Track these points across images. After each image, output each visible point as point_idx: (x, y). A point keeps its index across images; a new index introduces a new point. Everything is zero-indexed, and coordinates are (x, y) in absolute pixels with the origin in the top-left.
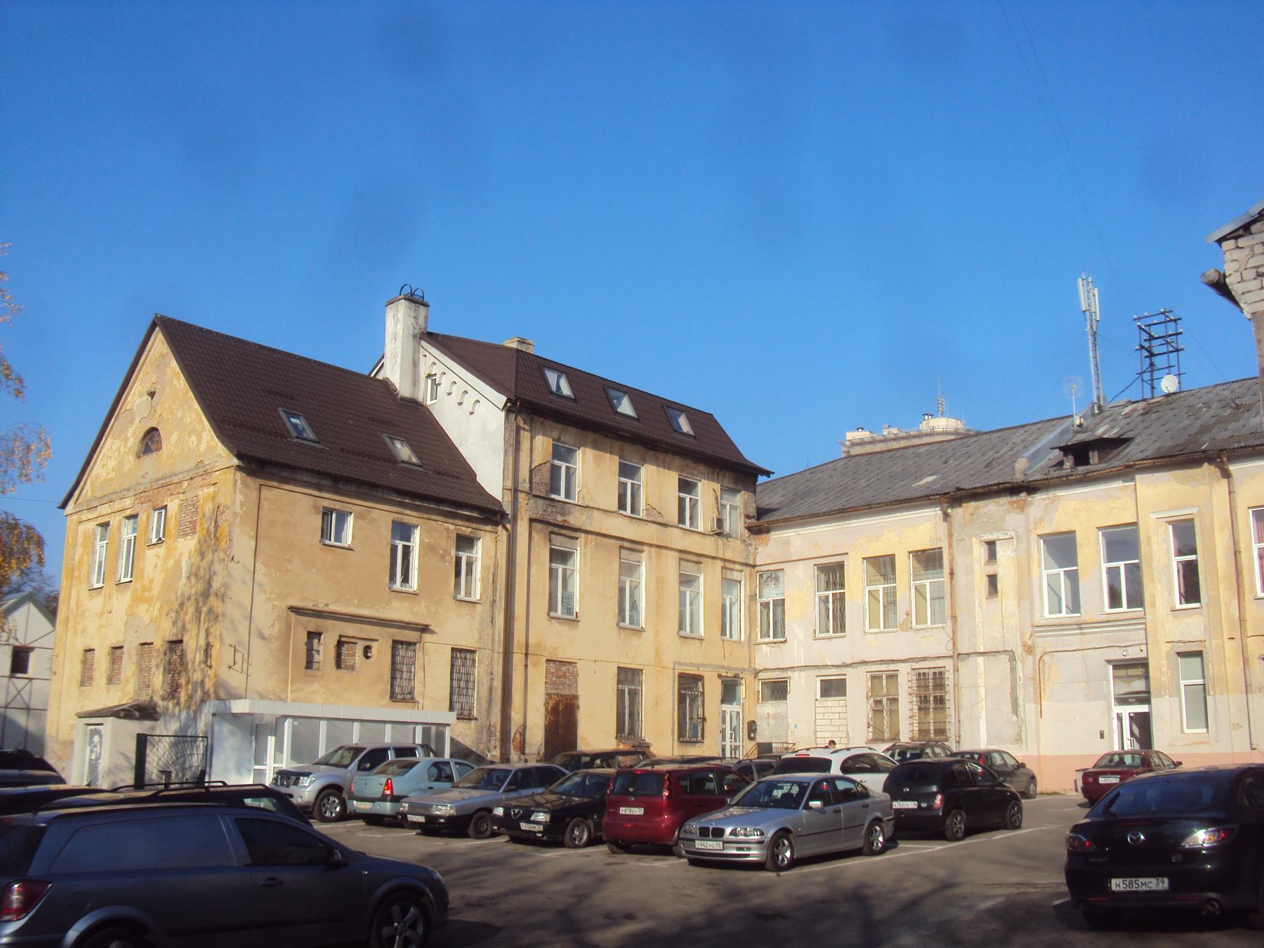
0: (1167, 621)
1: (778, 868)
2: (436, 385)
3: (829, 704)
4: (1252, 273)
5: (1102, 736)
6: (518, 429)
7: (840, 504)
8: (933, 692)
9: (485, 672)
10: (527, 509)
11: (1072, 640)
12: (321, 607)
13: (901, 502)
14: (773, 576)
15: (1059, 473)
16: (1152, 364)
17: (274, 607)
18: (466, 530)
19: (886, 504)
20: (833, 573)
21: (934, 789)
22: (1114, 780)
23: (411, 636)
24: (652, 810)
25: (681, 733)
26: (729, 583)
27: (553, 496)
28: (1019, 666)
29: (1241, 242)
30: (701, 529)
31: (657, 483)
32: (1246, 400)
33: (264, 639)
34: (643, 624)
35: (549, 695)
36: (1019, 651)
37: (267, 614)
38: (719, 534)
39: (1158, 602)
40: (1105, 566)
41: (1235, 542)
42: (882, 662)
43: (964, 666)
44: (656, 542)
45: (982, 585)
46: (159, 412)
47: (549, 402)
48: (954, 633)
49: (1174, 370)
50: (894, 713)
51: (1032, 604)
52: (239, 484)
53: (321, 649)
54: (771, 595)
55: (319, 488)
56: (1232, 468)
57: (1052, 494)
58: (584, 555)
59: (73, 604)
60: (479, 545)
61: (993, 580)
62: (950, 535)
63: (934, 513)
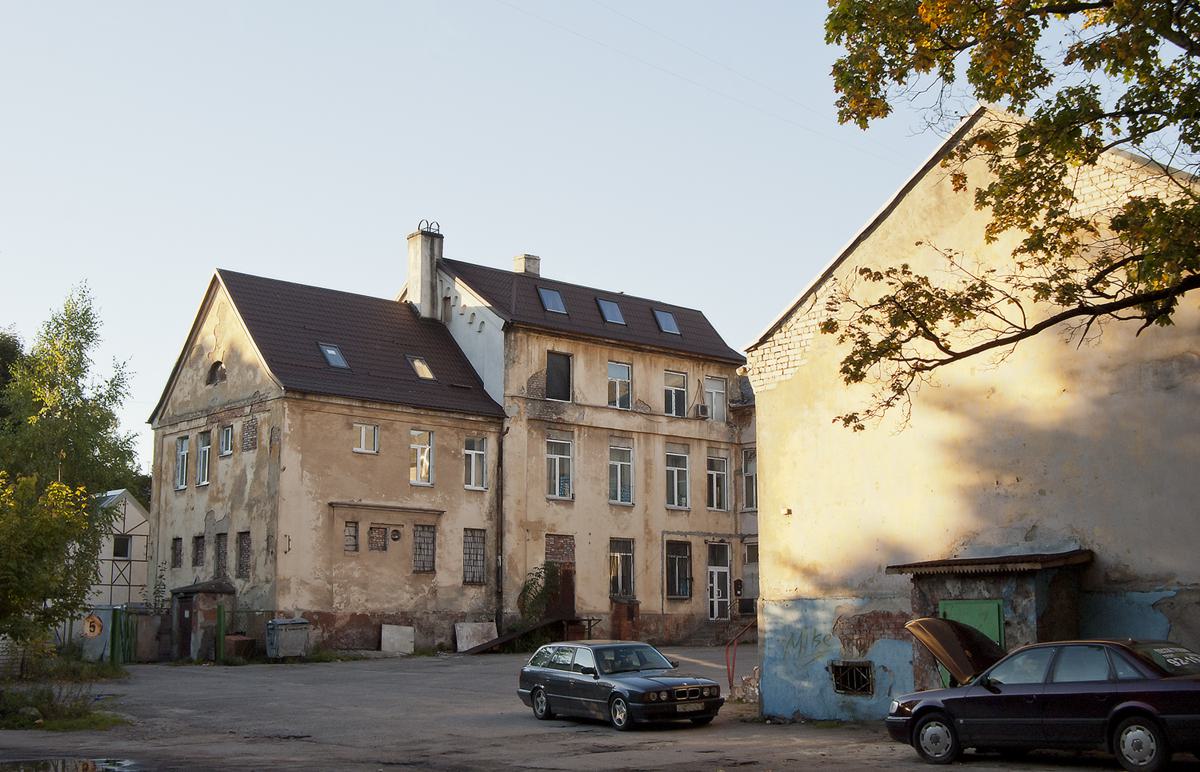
17: (318, 503)
23: (429, 520)
59: (163, 503)
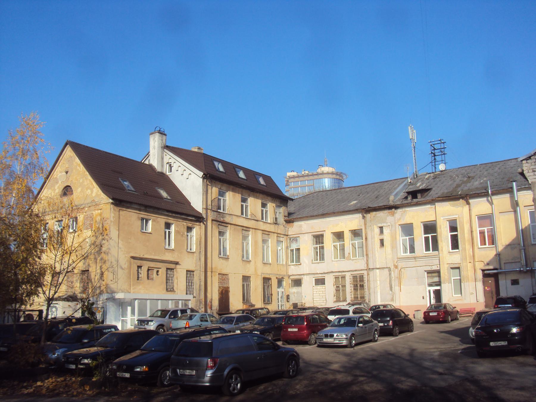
0: (446, 255)
1: (352, 347)
2: (171, 167)
3: (319, 288)
4: (532, 170)
5: (423, 298)
6: (207, 185)
7: (321, 212)
8: (359, 283)
9: (198, 278)
10: (211, 216)
11: (412, 263)
12: (141, 256)
13: (347, 211)
14: (295, 239)
15: (406, 202)
16: (435, 159)
18: (190, 225)
19: (341, 212)
20: (319, 238)
21: (388, 319)
22: (435, 314)
23: (172, 266)
24: (300, 329)
25: (264, 301)
26: (279, 242)
27: (219, 211)
28: (393, 273)
29: (528, 161)
30: (269, 222)
31: (254, 204)
32: (471, 175)
33: (123, 269)
34: (250, 258)
35: (220, 287)
36: (392, 268)
37: (124, 260)
38: (276, 224)
39: (444, 249)
40: (424, 236)
41: (471, 228)
42: (339, 272)
43: (371, 273)
44: (254, 227)
45: (378, 243)
46: (71, 179)
47: (220, 176)
48: (367, 261)
49: (444, 162)
50: (344, 291)
51: (397, 250)
52: (112, 210)
53: (142, 272)
54: (294, 246)
55: (140, 210)
56: (471, 201)
57: (404, 209)
58: (230, 233)
60: (194, 231)
61: (382, 242)
62: (365, 224)
63: (359, 216)
